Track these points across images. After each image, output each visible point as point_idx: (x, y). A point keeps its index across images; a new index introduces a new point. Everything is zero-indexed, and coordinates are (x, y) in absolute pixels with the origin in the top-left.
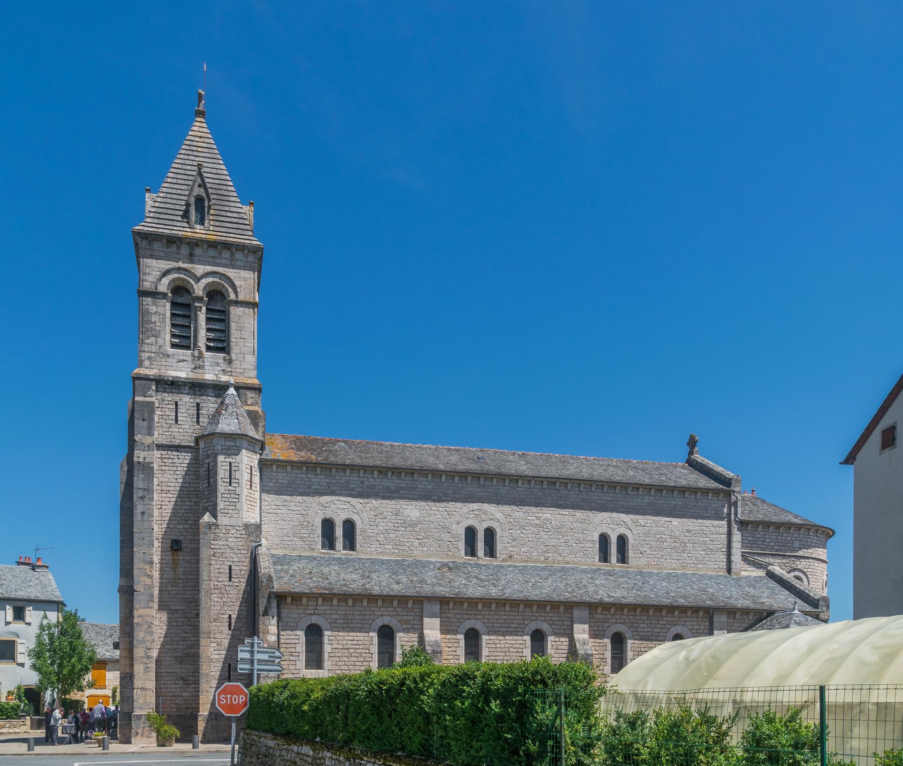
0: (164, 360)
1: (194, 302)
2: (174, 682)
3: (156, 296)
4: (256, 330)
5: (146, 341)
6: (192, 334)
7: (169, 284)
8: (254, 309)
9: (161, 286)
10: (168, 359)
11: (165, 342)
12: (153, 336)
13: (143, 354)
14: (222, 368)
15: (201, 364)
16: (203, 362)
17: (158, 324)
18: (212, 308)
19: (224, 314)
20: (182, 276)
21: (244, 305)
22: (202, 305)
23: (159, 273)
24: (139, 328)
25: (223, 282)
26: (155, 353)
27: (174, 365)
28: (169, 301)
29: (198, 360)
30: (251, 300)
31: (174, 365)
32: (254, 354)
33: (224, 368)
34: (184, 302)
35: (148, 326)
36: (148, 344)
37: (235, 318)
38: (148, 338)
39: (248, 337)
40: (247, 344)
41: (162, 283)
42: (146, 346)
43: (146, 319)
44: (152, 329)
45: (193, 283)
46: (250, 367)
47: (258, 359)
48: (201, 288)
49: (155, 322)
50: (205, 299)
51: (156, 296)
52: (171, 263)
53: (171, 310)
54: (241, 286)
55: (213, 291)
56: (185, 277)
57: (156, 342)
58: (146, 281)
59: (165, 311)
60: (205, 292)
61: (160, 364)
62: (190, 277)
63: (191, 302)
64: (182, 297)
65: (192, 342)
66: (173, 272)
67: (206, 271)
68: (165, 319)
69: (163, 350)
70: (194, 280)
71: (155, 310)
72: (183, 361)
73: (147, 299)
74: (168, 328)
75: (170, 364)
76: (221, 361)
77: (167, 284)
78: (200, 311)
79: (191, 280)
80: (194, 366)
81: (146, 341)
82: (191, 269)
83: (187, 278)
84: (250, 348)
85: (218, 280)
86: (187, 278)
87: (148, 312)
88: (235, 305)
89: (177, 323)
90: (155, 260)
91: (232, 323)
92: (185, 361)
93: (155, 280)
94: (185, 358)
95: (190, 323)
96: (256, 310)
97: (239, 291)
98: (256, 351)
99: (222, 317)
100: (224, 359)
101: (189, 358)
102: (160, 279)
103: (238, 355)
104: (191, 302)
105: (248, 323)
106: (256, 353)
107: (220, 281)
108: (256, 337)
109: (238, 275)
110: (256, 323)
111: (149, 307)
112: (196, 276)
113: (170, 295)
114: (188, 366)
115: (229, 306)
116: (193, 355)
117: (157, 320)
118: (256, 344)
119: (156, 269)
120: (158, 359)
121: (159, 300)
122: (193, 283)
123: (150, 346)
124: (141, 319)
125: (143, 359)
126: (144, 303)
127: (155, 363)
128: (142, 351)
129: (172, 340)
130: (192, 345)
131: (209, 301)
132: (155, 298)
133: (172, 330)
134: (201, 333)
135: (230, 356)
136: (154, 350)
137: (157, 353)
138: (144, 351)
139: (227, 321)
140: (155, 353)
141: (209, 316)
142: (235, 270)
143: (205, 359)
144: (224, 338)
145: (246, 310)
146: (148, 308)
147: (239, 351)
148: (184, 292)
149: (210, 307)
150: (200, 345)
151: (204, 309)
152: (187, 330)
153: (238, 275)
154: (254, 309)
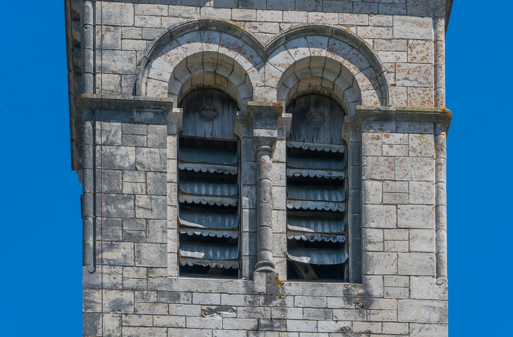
0: (161, 309)
1: (250, 126)
2: (89, 173)
3: (135, 114)
4: (444, 200)
5: (107, 255)
6: (246, 228)
7: (175, 77)
8: (436, 135)
9: (151, 83)
10: (173, 306)
11: (163, 254)
12: (128, 237)
13: (97, 296)
14: (341, 325)
15: (277, 314)
16: (283, 308)
17: (143, 200)
18: (305, 145)
19: (341, 166)
20: (214, 48)
21: (406, 125)
22: (275, 134)
23: (142, 45)
24: (84, 217)
25: (340, 59)
26: (133, 290)
27: (193, 322)
28: (175, 130)
29: (267, 302)
30: (429, 107)
31: (193, 322)
32: (438, 275)
33: (348, 324)
34: (218, 135)
35: (112, 210)
36: (112, 264)
37: (376, 165)
38: (111, 247)
39: (422, 225)
40: (417, 245)
41: (153, 73)
42: (105, 269)
43: (105, 188)
44: (125, 218)
45: (247, 66)
46: (425, 315)
47: (451, 289)
48: (273, 82)
49: (133, 195)
50: (284, 115)
51: (135, 114)
52: (178, 9)
53: (179, 161)
54: (395, 65)
55: (305, 95)
56: (223, 50)
57: (138, 255)
58: (103, 70)
59: (164, 159)
60: (285, 96)
61: (149, 323)
62: (239, 50)
63: (241, 131)
64: (210, 119)
65: (246, 228)
66: (187, 37)
67: (286, 27)
68: (163, 182)
69: (157, 281)
70: (250, 59)
71: (132, 158)
72: (220, 309)
73: (107, 125)
74: (172, 213)
75: (181, 321)
76: (337, 302)
77: (167, 77)
78: (270, 152)
79: (241, 59)
80: (252, 324)
81: (107, 255)
82: (241, 25)
83: (231, 54)
84: (427, 257)
85: (324, 53)
86: (231, 54)
87: (112, 166)
88: (377, 126)
89: (197, 200)
90: (130, 5)
91: (368, 184)
92: (227, 308)
93: (131, 67)
94: (226, 300)
95: (238, 196)
96: (443, 136)
97: (390, 81)
98: (445, 265)
99: (335, 174)
100: (348, 297)
101: (238, 300)
102: (148, 62)
103: (390, 281)
104: (241, 131)
105: (421, 179)
106: (445, 272)
107: (330, 55)
108: (444, 220)
109: (385, 33)
110: (443, 178)
111: (113, 149)
112: (255, 45)
113: (176, 110)
114: (236, 323)
115: (358, 132)
116: (252, 292)
117: (139, 188)
118: (445, 244)
119: (135, 33)
120: (144, 308)
121: (142, 128)
122: (247, 66)
123: (119, 269)
124: (89, 188)
125: (99, 309)
126: (98, 140)
127: (134, 320)
128: (94, 287)
129: (183, 253)
130: (246, 263)
131: (295, 123)
132: (132, 121)
133: (183, 222)
134: (274, 223)
135: (366, 286)
136: (130, 283)
137: (141, 290)
138: (101, 287)
139: (350, 184)
140: (133, 290)
141: (296, 173)
142: (376, 19)
143: (289, 301)
144: (340, 239)
145: (414, 140)
146: (112, 155)
147: (392, 269)
148: (218, 105)
149: (297, 145)
150: (270, 256)
151: (281, 147)
152: (228, 222)
153: (385, 33)
154: (436, 135)
